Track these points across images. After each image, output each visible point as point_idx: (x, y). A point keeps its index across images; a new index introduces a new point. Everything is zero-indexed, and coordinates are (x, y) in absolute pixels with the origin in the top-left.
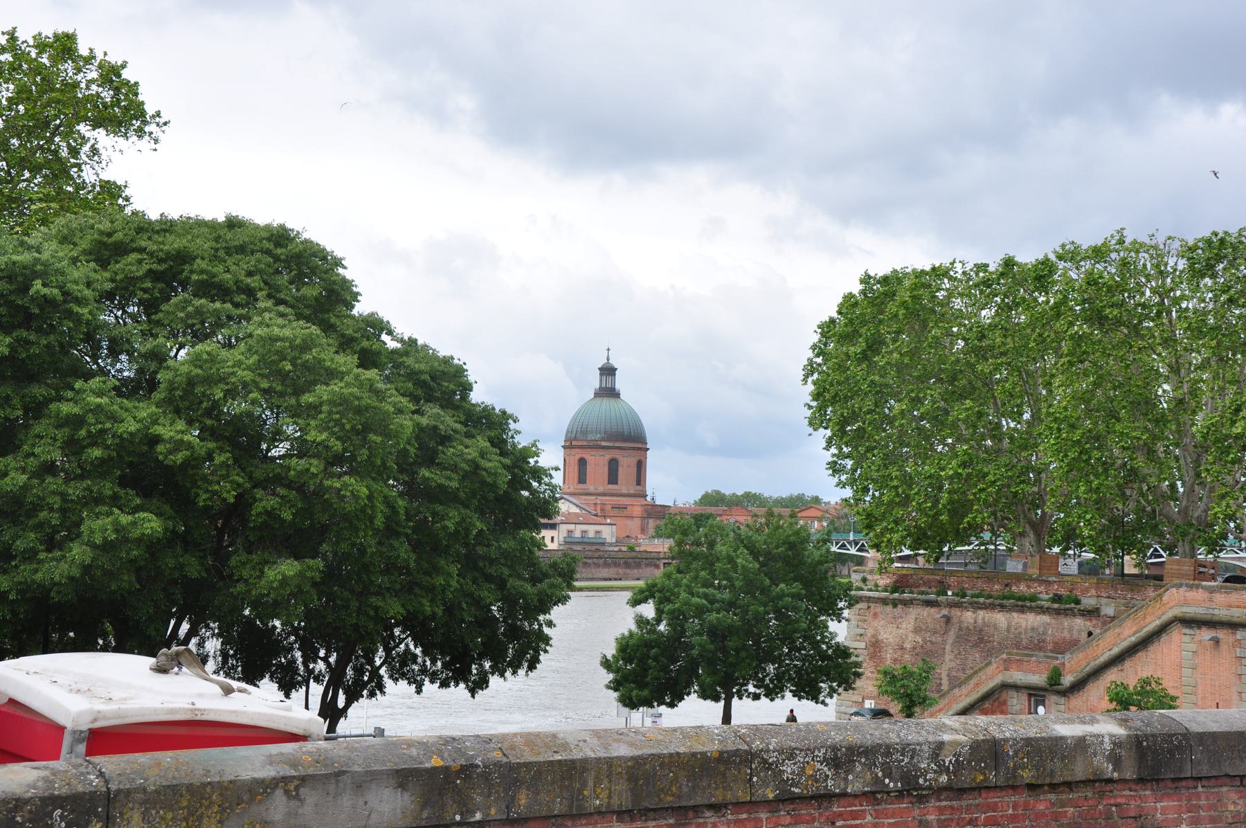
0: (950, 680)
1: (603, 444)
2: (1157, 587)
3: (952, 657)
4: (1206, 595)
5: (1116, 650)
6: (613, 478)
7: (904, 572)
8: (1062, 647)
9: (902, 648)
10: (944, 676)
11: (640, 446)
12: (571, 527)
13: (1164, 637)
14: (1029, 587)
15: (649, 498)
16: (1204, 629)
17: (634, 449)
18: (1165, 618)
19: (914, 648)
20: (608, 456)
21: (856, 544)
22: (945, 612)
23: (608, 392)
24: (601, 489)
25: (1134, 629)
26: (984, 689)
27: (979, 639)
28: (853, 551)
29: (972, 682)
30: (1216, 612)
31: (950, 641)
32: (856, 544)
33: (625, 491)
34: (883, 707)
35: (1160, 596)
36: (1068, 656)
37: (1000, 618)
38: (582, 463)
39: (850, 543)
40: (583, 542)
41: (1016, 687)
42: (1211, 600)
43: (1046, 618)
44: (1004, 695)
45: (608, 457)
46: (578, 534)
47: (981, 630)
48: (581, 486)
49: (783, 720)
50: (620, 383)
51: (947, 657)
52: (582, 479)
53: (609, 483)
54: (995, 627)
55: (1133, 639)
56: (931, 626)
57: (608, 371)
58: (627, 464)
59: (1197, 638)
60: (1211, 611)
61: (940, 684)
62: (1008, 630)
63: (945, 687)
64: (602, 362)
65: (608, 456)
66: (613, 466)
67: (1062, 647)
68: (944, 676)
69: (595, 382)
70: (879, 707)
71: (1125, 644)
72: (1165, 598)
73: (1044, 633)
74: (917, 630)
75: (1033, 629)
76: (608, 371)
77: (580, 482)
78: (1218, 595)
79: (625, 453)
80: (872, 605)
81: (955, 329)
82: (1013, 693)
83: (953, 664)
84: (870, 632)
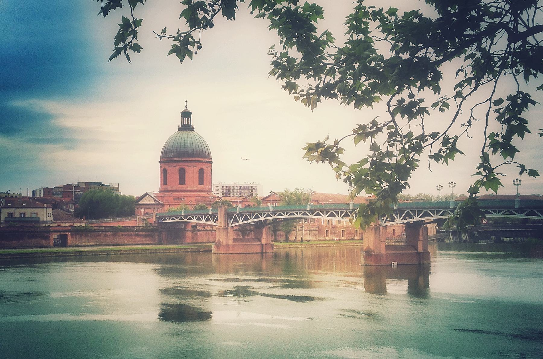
1: (175, 159)
23: (186, 127)
45: (178, 167)
50: (194, 121)
57: (186, 115)
64: (183, 109)
69: (178, 121)
76: (186, 115)
79: (190, 164)
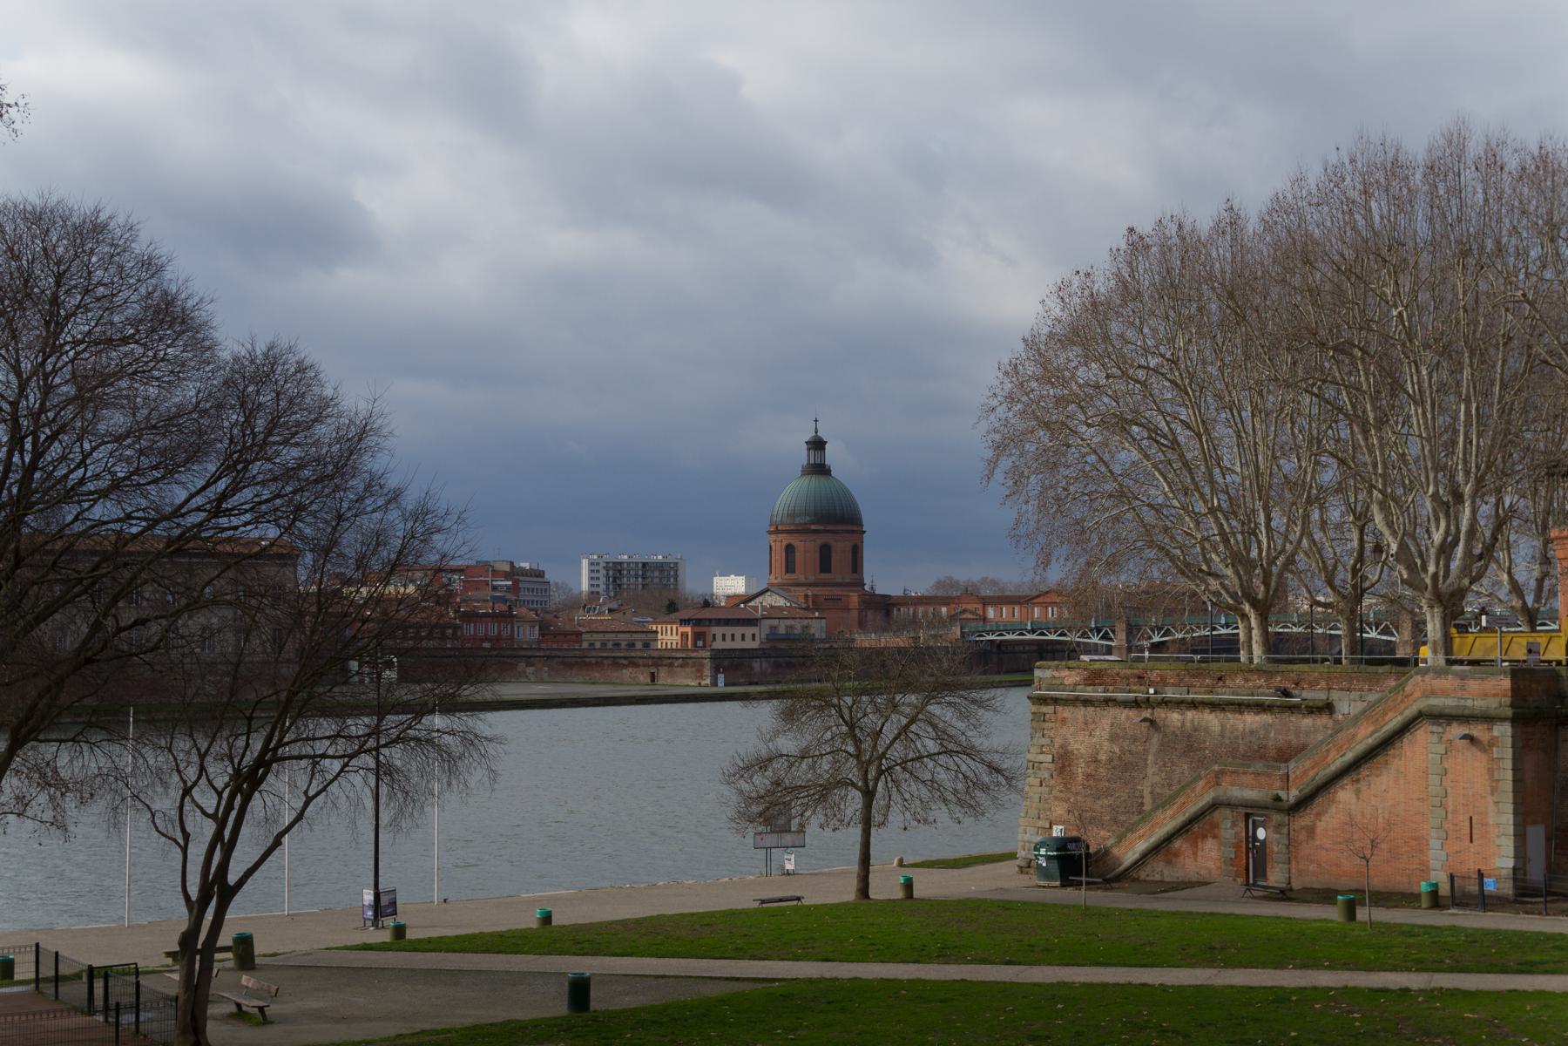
0: (1154, 800)
2: (1399, 675)
3: (1155, 769)
4: (1458, 682)
5: (1350, 756)
6: (825, 566)
7: (1097, 666)
8: (1285, 755)
9: (1096, 761)
10: (1146, 793)
11: (850, 528)
12: (775, 622)
13: (1407, 739)
14: (1247, 680)
15: (867, 588)
16: (1455, 724)
17: (847, 532)
18: (1410, 712)
19: (1110, 760)
20: (820, 540)
21: (1099, 631)
22: (1147, 714)
23: (819, 469)
24: (812, 579)
25: (1371, 729)
26: (1192, 809)
27: (1188, 745)
28: (1095, 640)
29: (1179, 801)
30: (1469, 703)
31: (1153, 750)
32: (1099, 631)
33: (839, 580)
34: (1075, 834)
35: (1402, 686)
36: (1292, 764)
37: (1212, 720)
38: (790, 549)
39: (1370, 625)
40: (788, 638)
41: (1229, 805)
42: (1463, 688)
43: (1266, 718)
44: (1217, 815)
46: (782, 631)
47: (1189, 736)
48: (789, 576)
49: (534, 925)
50: (832, 455)
51: (1150, 771)
52: (790, 568)
53: (822, 571)
54: (1207, 730)
55: (1370, 741)
56: (1130, 732)
58: (840, 548)
59: (1447, 736)
60: (1462, 702)
61: (1142, 804)
62: (1222, 734)
63: (1147, 807)
64: (809, 436)
65: (820, 540)
66: (825, 554)
67: (1285, 755)
68: (1146, 793)
69: (802, 456)
70: (1069, 834)
71: (1360, 748)
72: (1408, 688)
73: (1266, 737)
74: (1114, 738)
75: (1252, 732)
76: (817, 445)
77: (787, 571)
78: (1471, 682)
80: (1060, 708)
81: (1528, 435)
82: (1227, 812)
83: (1157, 779)
84: (1058, 742)
